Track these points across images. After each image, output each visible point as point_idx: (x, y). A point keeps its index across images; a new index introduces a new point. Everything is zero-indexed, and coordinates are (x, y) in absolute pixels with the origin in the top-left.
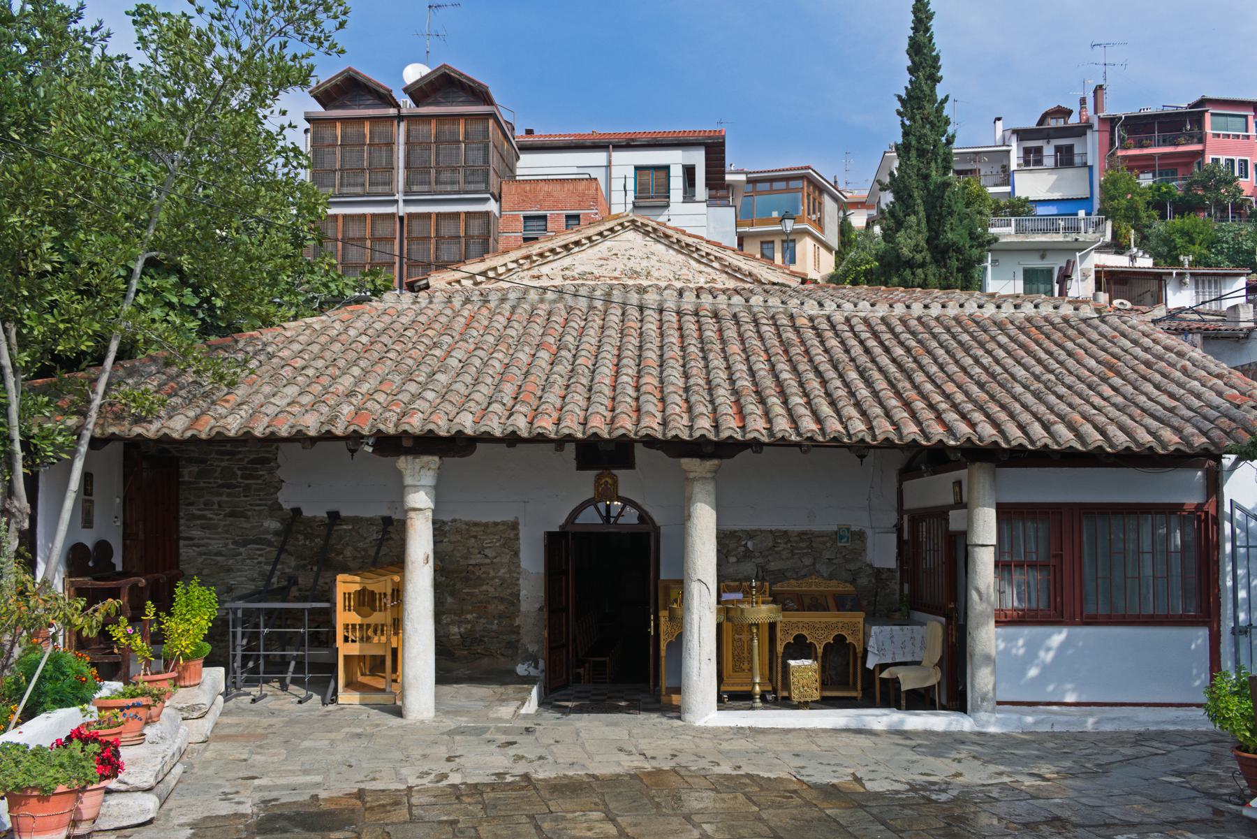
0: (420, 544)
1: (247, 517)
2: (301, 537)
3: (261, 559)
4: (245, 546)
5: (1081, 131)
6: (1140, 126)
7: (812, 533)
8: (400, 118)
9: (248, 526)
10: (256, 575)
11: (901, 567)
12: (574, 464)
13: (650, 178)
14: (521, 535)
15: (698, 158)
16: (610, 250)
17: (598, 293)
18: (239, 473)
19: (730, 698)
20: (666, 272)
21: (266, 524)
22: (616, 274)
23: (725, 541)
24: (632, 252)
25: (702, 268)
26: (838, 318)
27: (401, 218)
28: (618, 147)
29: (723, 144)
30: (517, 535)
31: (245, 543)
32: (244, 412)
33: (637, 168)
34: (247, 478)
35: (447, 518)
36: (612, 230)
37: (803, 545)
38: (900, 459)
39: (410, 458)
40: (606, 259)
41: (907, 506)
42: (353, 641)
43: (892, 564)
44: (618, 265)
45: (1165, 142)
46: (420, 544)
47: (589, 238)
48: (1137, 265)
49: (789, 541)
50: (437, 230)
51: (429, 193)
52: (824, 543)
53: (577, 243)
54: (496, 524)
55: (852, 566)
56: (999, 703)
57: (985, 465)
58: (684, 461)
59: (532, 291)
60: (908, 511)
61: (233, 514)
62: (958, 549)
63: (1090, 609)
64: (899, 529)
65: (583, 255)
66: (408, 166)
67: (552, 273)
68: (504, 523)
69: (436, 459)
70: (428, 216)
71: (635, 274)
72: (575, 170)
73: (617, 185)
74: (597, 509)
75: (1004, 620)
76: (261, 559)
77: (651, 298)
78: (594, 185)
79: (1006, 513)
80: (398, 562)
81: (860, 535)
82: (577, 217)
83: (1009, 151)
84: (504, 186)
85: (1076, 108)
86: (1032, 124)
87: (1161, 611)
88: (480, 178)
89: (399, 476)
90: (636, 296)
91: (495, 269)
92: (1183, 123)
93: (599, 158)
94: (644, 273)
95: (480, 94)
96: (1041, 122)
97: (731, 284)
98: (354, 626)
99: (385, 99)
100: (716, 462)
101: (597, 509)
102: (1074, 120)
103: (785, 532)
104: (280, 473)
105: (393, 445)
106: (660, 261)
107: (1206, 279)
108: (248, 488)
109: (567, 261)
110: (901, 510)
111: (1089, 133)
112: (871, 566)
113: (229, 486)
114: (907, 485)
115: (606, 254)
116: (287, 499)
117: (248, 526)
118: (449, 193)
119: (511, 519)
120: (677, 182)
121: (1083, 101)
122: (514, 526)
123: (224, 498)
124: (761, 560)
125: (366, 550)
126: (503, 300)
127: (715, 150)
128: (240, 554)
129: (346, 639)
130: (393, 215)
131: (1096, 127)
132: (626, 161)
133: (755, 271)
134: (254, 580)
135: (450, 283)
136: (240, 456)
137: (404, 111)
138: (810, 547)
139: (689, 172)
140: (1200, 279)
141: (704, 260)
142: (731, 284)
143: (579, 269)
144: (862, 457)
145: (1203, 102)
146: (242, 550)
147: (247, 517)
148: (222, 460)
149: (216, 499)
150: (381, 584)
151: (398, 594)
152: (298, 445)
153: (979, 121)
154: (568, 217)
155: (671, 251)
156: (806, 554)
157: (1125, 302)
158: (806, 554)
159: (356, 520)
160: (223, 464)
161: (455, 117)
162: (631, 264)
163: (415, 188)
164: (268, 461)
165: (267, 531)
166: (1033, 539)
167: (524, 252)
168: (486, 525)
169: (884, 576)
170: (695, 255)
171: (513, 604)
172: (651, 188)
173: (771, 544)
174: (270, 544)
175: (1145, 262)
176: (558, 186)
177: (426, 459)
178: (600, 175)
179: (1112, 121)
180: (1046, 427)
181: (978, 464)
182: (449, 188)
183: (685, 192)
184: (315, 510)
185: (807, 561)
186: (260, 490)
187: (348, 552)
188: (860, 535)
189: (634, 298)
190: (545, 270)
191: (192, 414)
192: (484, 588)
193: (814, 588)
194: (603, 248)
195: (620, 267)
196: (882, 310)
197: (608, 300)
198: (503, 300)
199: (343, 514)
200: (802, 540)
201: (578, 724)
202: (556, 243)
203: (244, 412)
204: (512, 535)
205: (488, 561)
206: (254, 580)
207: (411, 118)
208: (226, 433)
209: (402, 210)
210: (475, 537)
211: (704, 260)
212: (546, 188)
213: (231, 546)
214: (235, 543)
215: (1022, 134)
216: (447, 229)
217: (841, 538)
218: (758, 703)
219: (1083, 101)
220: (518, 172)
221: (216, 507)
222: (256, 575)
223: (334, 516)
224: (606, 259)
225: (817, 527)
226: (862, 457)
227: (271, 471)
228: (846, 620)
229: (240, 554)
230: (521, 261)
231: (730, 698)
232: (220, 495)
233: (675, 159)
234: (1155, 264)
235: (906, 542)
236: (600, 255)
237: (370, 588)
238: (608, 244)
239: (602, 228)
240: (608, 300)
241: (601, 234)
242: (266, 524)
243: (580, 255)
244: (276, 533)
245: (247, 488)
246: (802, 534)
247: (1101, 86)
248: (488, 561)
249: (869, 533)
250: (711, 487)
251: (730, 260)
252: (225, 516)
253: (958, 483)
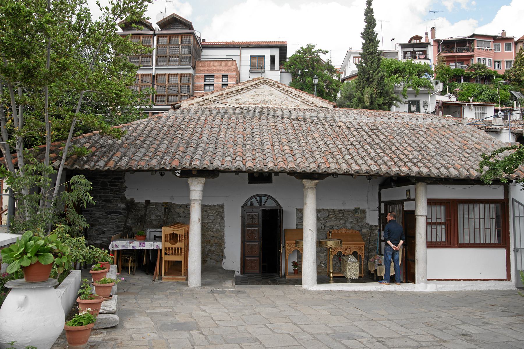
0: (196, 215)
1: (111, 202)
2: (133, 211)
3: (117, 220)
4: (110, 214)
5: (426, 45)
6: (448, 45)
7: (344, 210)
8: (154, 35)
9: (112, 206)
10: (114, 227)
11: (380, 225)
12: (247, 181)
13: (256, 61)
14: (225, 210)
15: (276, 53)
16: (255, 92)
17: (257, 111)
18: (108, 183)
19: (322, 279)
20: (279, 101)
21: (119, 205)
22: (258, 102)
23: (322, 215)
24: (265, 94)
25: (293, 100)
26: (355, 123)
27: (154, 76)
28: (243, 47)
29: (286, 47)
30: (223, 210)
31: (110, 213)
32: (126, 159)
33: (251, 56)
34: (112, 186)
35: (429, 198)
36: (256, 84)
37: (341, 215)
38: (379, 181)
39: (194, 179)
40: (254, 96)
41: (382, 200)
42: (168, 255)
43: (377, 223)
44: (258, 99)
45: (459, 52)
46: (196, 215)
47: (247, 87)
48: (452, 100)
49: (335, 214)
50: (169, 81)
51: (166, 66)
52: (349, 214)
53: (242, 89)
54: (214, 206)
55: (360, 224)
56: (428, 280)
57: (423, 183)
58: (304, 180)
59: (238, 109)
60: (383, 202)
61: (106, 201)
62: (410, 218)
63: (461, 241)
64: (379, 208)
65: (245, 94)
66: (157, 54)
67: (232, 102)
68: (218, 205)
69: (204, 179)
70: (165, 75)
71: (265, 102)
72: (225, 57)
73: (243, 63)
74: (257, 200)
75: (430, 245)
76: (117, 220)
77: (279, 113)
78: (234, 63)
79: (431, 202)
80: (186, 221)
81: (364, 211)
82: (227, 76)
83: (398, 52)
84: (197, 63)
85: (424, 36)
86: (406, 41)
87: (472, 242)
88: (187, 60)
89: (188, 186)
90: (273, 112)
91: (208, 99)
92: (464, 44)
93: (236, 52)
94: (269, 102)
95: (188, 25)
96: (410, 41)
97: (305, 107)
98: (169, 248)
99: (149, 27)
100: (317, 181)
101: (257, 200)
102: (423, 41)
103: (333, 210)
104: (126, 184)
105: (188, 173)
106: (276, 97)
107: (479, 107)
108: (112, 190)
109: (238, 97)
110: (380, 202)
111: (429, 46)
112: (368, 224)
113: (104, 189)
114: (382, 191)
115: (254, 94)
116: (128, 195)
117: (112, 206)
118: (173, 66)
119: (221, 204)
120: (267, 62)
121: (427, 33)
122: (222, 207)
123: (102, 194)
124: (323, 221)
125: (160, 216)
126: (218, 113)
127: (283, 49)
128: (108, 218)
129: (165, 254)
130: (150, 75)
131: (432, 44)
132: (247, 53)
133: (314, 102)
134: (113, 229)
135: (189, 105)
136: (109, 177)
137: (156, 32)
138: (343, 216)
139: (273, 59)
140: (477, 107)
141: (294, 97)
142: (305, 107)
143: (243, 100)
144: (369, 179)
145: (474, 35)
146: (109, 216)
147: (111, 202)
148: (101, 178)
149: (98, 195)
150: (179, 231)
151: (187, 235)
152: (150, 173)
153: (390, 40)
154: (223, 76)
155: (280, 93)
156: (341, 219)
157: (450, 116)
158: (341, 219)
159: (156, 204)
160: (102, 180)
161: (177, 35)
162: (264, 98)
163: (160, 63)
164: (121, 179)
165: (119, 208)
166: (440, 213)
167: (220, 93)
168: (210, 206)
169: (373, 228)
170: (290, 95)
171: (221, 239)
172: (257, 64)
173: (327, 215)
174: (121, 213)
175: (454, 99)
176: (219, 63)
177: (200, 179)
178: (236, 59)
179: (438, 42)
180: (447, 168)
181: (420, 183)
182: (174, 63)
183: (271, 67)
184: (140, 199)
185: (342, 222)
186: (117, 191)
187: (153, 217)
188: (364, 211)
189: (272, 113)
190: (229, 100)
191: (106, 160)
192: (210, 233)
193: (344, 233)
194: (253, 91)
195: (260, 99)
196: (372, 120)
197: (261, 113)
198: (218, 113)
199: (152, 201)
200: (340, 213)
201: (261, 289)
202: (233, 89)
203: (126, 159)
204: (221, 211)
205: (211, 221)
206: (113, 229)
207: (159, 35)
208: (122, 168)
209: (153, 72)
210: (206, 211)
211: (294, 97)
212: (214, 64)
213: (104, 214)
214: (106, 213)
215: (403, 46)
216: (173, 80)
217: (356, 212)
218: (332, 281)
219: (427, 33)
220: (202, 57)
221: (98, 198)
222: (114, 227)
223: (148, 202)
224: (254, 96)
225: (346, 208)
226: (369, 179)
227: (122, 183)
228: (357, 245)
229: (108, 218)
230: (219, 97)
231: (322, 279)
232: (101, 193)
233: (267, 53)
234: (457, 100)
235: (383, 214)
236: (251, 94)
237: (176, 233)
238: (255, 90)
239: (252, 83)
240: (261, 113)
241: (252, 86)
242: (119, 205)
243: (243, 94)
244: (124, 209)
245: (112, 190)
246: (340, 211)
247: (433, 28)
248: (211, 221)
249: (367, 210)
250: (315, 191)
251: (305, 97)
252: (102, 201)
253: (409, 191)
